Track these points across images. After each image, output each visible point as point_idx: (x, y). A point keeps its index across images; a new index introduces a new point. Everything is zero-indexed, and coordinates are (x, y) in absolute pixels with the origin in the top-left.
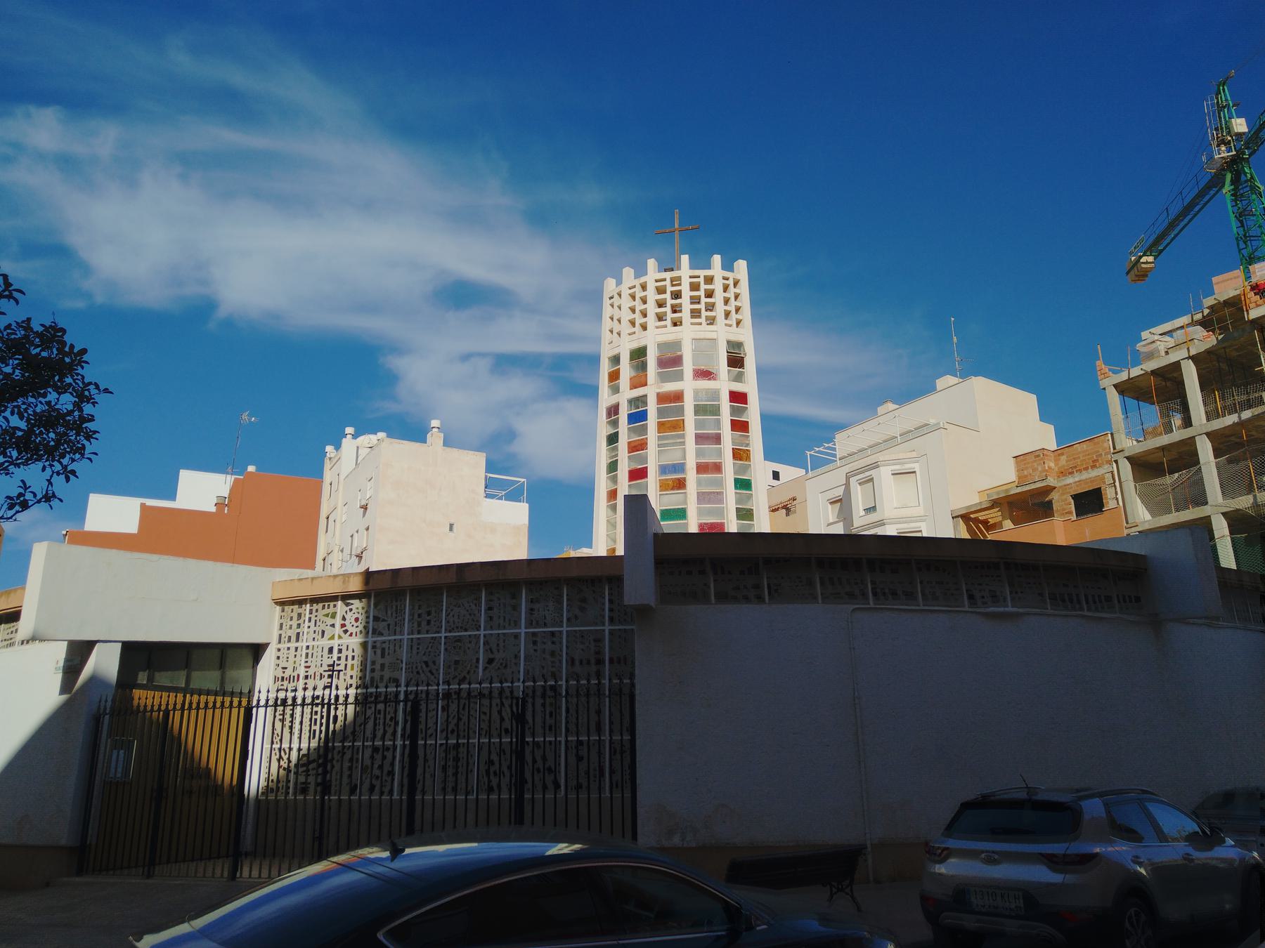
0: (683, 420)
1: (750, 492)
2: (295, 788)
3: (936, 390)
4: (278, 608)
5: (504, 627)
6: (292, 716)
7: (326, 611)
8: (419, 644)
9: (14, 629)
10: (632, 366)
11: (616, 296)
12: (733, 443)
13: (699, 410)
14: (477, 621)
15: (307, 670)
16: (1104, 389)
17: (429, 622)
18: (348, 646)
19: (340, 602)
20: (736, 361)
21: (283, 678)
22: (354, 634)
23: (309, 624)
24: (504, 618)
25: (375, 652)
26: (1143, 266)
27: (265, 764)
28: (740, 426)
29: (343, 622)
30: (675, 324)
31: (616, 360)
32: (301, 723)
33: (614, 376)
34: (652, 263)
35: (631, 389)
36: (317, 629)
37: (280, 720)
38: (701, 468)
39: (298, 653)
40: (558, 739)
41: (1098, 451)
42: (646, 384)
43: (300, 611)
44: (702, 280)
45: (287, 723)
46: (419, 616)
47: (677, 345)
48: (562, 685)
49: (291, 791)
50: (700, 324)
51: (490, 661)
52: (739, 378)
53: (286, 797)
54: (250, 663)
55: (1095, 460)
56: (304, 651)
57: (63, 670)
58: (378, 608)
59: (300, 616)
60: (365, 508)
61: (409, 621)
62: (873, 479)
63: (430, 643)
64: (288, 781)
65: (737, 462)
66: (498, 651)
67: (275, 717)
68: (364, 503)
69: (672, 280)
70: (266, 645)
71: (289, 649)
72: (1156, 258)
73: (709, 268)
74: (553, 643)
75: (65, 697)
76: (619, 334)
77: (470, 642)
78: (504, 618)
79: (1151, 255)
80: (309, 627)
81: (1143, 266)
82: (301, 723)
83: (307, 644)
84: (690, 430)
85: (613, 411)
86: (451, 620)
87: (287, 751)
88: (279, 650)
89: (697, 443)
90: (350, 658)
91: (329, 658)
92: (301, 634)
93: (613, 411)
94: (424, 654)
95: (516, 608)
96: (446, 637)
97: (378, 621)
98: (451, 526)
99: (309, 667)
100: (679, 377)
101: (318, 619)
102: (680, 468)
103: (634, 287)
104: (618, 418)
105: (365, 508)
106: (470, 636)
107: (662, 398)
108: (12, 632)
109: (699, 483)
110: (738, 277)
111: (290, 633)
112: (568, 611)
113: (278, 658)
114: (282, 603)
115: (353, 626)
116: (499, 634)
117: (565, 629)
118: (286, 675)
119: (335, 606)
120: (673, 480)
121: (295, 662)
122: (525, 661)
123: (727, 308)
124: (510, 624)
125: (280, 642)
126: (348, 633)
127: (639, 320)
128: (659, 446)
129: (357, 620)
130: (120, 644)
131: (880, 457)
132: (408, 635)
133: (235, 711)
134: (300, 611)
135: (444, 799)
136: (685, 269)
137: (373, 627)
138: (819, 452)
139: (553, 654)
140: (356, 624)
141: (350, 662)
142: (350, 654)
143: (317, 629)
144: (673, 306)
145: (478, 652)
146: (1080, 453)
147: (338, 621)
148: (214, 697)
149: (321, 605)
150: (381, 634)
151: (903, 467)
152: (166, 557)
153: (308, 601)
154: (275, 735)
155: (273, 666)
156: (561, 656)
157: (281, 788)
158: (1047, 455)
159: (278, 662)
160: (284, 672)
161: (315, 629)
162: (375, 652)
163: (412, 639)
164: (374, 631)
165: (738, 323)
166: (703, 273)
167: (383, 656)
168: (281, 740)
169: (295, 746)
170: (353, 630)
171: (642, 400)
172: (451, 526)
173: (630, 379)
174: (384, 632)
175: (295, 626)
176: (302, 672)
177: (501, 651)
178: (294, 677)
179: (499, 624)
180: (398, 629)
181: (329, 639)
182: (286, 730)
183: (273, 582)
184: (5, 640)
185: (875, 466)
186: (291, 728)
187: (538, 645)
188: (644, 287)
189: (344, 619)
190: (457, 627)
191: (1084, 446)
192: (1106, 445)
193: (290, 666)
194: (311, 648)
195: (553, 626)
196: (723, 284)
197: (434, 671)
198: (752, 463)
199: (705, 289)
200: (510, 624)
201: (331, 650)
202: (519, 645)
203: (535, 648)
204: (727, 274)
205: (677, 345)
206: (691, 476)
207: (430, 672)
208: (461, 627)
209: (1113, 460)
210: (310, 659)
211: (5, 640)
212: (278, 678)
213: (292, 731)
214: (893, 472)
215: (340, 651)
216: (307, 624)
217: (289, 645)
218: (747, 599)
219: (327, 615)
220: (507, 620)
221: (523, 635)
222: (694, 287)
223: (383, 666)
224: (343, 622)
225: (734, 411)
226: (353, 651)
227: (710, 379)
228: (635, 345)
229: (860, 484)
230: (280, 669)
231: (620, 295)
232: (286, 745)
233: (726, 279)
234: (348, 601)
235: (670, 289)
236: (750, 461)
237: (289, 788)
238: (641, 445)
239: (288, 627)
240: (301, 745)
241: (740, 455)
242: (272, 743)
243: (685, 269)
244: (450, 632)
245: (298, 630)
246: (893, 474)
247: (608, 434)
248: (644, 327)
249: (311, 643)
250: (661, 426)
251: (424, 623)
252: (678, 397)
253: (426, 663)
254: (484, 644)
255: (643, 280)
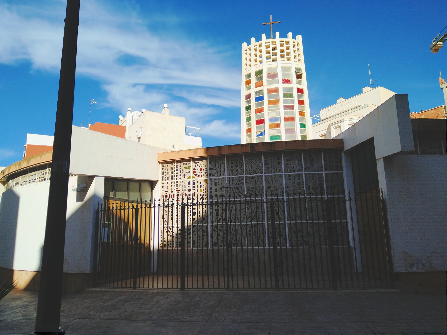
0: (279, 100)
1: (305, 129)
2: (177, 244)
3: (363, 93)
4: (161, 165)
5: (274, 172)
6: (172, 212)
7: (185, 166)
8: (233, 180)
9: (44, 173)
10: (256, 78)
11: (248, 50)
12: (299, 109)
13: (285, 96)
14: (261, 169)
15: (178, 192)
16: (442, 89)
17: (237, 170)
18: (197, 181)
19: (192, 162)
20: (299, 76)
21: (166, 196)
22: (200, 176)
23: (177, 172)
24: (274, 168)
25: (211, 184)
26: (438, 46)
27: (161, 234)
28: (301, 102)
29: (194, 171)
30: (273, 61)
31: (249, 76)
32: (177, 215)
33: (248, 83)
34: (264, 36)
35: (256, 87)
36: (181, 174)
37: (166, 214)
38: (286, 119)
39: (173, 185)
40: (212, 224)
41: (439, 113)
42: (263, 85)
43: (172, 166)
44: (284, 43)
45: (170, 216)
46: (232, 167)
47: (275, 68)
48: (325, 197)
49: (175, 245)
50: (284, 61)
51: (269, 187)
52: (299, 83)
53: (172, 248)
54: (150, 189)
55: (437, 117)
56: (176, 184)
57: (77, 190)
58: (211, 164)
59: (172, 168)
60: (139, 138)
61: (227, 170)
62: (341, 126)
63: (239, 179)
64: (173, 241)
65: (300, 117)
66: (272, 183)
67: (164, 213)
68: (139, 137)
69: (272, 43)
70: (157, 181)
71: (168, 183)
72: (443, 42)
73: (287, 37)
74: (299, 179)
75: (80, 204)
76: (250, 66)
77: (258, 179)
78: (274, 168)
79: (442, 41)
80: (177, 173)
81: (438, 46)
82: (177, 215)
83: (177, 181)
84: (282, 104)
85: (248, 97)
86: (248, 169)
87: (171, 228)
88: (163, 184)
89: (284, 109)
90: (199, 186)
91: (188, 186)
92: (173, 176)
93: (248, 97)
94: (236, 184)
95: (280, 163)
96: (246, 177)
97: (212, 170)
98: (173, 146)
99: (179, 191)
100: (277, 82)
101: (181, 169)
102: (277, 119)
103: (256, 45)
104: (251, 100)
105: (139, 138)
106: (258, 176)
107: (270, 91)
108: (43, 174)
109: (285, 125)
110: (299, 42)
111: (167, 176)
112: (305, 165)
113: (163, 187)
114: (162, 163)
115: (198, 171)
116: (272, 175)
117: (304, 173)
118: (168, 194)
119: (189, 164)
120: (275, 124)
121: (171, 189)
122: (286, 187)
123: (295, 54)
124: (277, 171)
125: (163, 180)
126: (197, 176)
127: (259, 59)
128: (269, 110)
129: (201, 169)
130: (104, 178)
131: (344, 118)
132: (227, 176)
133: (131, 211)
134: (172, 166)
135: (237, 249)
136: (278, 38)
137: (210, 172)
138: (316, 117)
139: (299, 184)
140: (201, 172)
141: (199, 188)
142: (199, 185)
143: (181, 174)
144: (273, 53)
145: (262, 183)
146: (430, 114)
147: (192, 170)
148: (132, 203)
149: (182, 163)
150: (213, 175)
151: (353, 122)
152: (119, 138)
153: (176, 162)
154: (165, 221)
155: (160, 191)
156: (303, 185)
157: (169, 245)
158: (416, 115)
159: (163, 189)
160: (166, 193)
161: (180, 174)
162: (211, 184)
163: (229, 178)
164: (210, 174)
165: (299, 60)
166: (285, 40)
167: (216, 185)
168: (168, 223)
169: (175, 225)
170: (200, 174)
171: (261, 92)
172: (173, 146)
173: (255, 83)
174: (215, 175)
175: (170, 173)
176: (176, 194)
177: (274, 183)
178: (171, 195)
179: (272, 171)
180: (222, 173)
181: (188, 178)
182: (170, 219)
183: (158, 154)
184: (40, 178)
185: (342, 121)
186: (172, 218)
187: (291, 180)
188: (260, 46)
189: (194, 169)
190: (251, 172)
191: (432, 111)
192: (442, 110)
193: (169, 190)
194: (179, 182)
195: (298, 171)
196: (293, 44)
197: (242, 192)
198: (306, 117)
199: (286, 47)
200: (277, 171)
201: (189, 183)
202: (282, 180)
203: (290, 181)
204: (294, 40)
205: (275, 68)
206: (283, 123)
207: (240, 192)
208: (253, 172)
209: (445, 116)
210: (179, 187)
211: (40, 178)
212: (164, 196)
213: (173, 219)
214: (349, 124)
215: (194, 183)
216: (176, 172)
217: (168, 181)
218: (435, 153)
219: (186, 168)
220: (275, 169)
221: (284, 176)
222: (282, 45)
223: (216, 190)
224: (194, 171)
225: (299, 96)
226: (201, 183)
227: (289, 83)
228: (258, 69)
229: (335, 128)
230: (164, 192)
231: (250, 50)
232: (170, 225)
233: (294, 42)
234: (196, 161)
235: (271, 46)
236: (305, 116)
237: (174, 244)
238: (261, 110)
239: (166, 173)
240: (178, 225)
241: (301, 114)
242: (163, 225)
243: (278, 38)
244: (248, 174)
245: (172, 175)
246: (349, 124)
247: (246, 106)
248: (261, 62)
249: (179, 180)
250: (270, 103)
251: (235, 171)
252: (276, 90)
253: (238, 189)
254: (265, 180)
255: (260, 42)
